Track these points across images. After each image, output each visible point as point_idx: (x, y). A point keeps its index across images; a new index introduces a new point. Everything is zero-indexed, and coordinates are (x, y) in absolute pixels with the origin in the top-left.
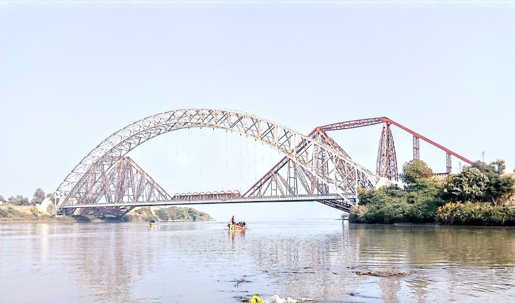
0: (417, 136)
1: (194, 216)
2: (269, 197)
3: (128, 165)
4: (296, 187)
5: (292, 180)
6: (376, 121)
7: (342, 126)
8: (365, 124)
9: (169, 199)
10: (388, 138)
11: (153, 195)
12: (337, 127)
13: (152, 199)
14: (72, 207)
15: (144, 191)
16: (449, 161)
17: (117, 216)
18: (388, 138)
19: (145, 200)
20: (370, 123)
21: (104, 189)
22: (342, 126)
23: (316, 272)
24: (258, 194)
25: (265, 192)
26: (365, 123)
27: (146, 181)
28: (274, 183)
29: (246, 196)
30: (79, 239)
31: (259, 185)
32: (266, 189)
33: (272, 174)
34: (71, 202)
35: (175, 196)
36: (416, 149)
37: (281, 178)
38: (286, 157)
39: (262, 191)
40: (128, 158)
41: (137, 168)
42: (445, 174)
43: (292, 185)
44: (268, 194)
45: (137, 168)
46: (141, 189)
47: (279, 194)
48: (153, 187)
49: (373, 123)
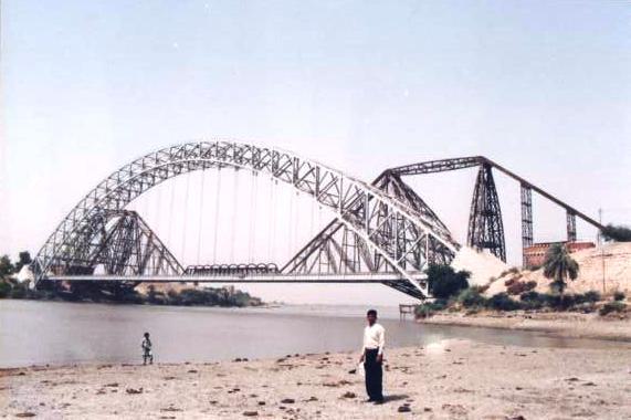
0: (526, 185)
3: (130, 222)
7: (423, 168)
10: (486, 185)
15: (151, 259)
17: (121, 295)
18: (486, 185)
19: (151, 273)
22: (423, 168)
23: (565, 384)
29: (287, 271)
31: (304, 255)
33: (322, 240)
36: (527, 205)
38: (336, 220)
43: (350, 257)
48: (162, 257)
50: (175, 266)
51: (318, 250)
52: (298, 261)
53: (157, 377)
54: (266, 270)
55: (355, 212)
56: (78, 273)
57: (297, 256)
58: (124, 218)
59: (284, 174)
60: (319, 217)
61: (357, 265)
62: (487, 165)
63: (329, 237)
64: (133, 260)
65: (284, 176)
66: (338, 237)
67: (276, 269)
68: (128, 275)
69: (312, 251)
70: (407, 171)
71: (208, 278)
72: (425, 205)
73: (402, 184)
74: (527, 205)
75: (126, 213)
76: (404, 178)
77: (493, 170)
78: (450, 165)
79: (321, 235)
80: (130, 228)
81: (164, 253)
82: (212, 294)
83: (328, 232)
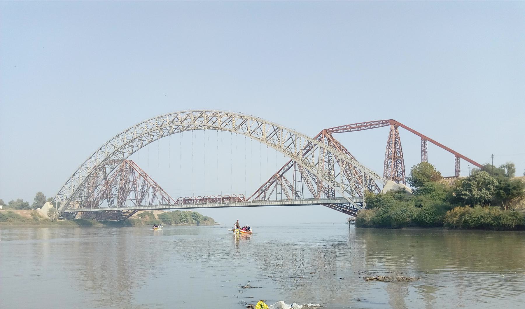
0: (425, 139)
1: (197, 220)
3: (128, 169)
4: (301, 191)
5: (298, 183)
6: (384, 123)
7: (348, 129)
8: (372, 127)
10: (395, 141)
12: (343, 129)
13: (155, 203)
14: (73, 211)
15: (147, 195)
16: (457, 164)
18: (395, 141)
19: (148, 204)
20: (378, 126)
21: (106, 194)
22: (348, 129)
24: (263, 198)
25: (270, 196)
27: (149, 185)
28: (279, 186)
29: (251, 200)
31: (264, 188)
32: (271, 193)
33: (277, 178)
35: (178, 200)
37: (286, 181)
39: (267, 195)
40: (131, 161)
44: (273, 197)
46: (143, 193)
47: (285, 198)
51: (276, 182)
52: (261, 192)
54: (236, 199)
56: (88, 207)
57: (260, 189)
62: (396, 124)
63: (281, 176)
64: (132, 195)
68: (129, 204)
76: (333, 135)
81: (156, 189)
82: (185, 216)
83: (281, 173)
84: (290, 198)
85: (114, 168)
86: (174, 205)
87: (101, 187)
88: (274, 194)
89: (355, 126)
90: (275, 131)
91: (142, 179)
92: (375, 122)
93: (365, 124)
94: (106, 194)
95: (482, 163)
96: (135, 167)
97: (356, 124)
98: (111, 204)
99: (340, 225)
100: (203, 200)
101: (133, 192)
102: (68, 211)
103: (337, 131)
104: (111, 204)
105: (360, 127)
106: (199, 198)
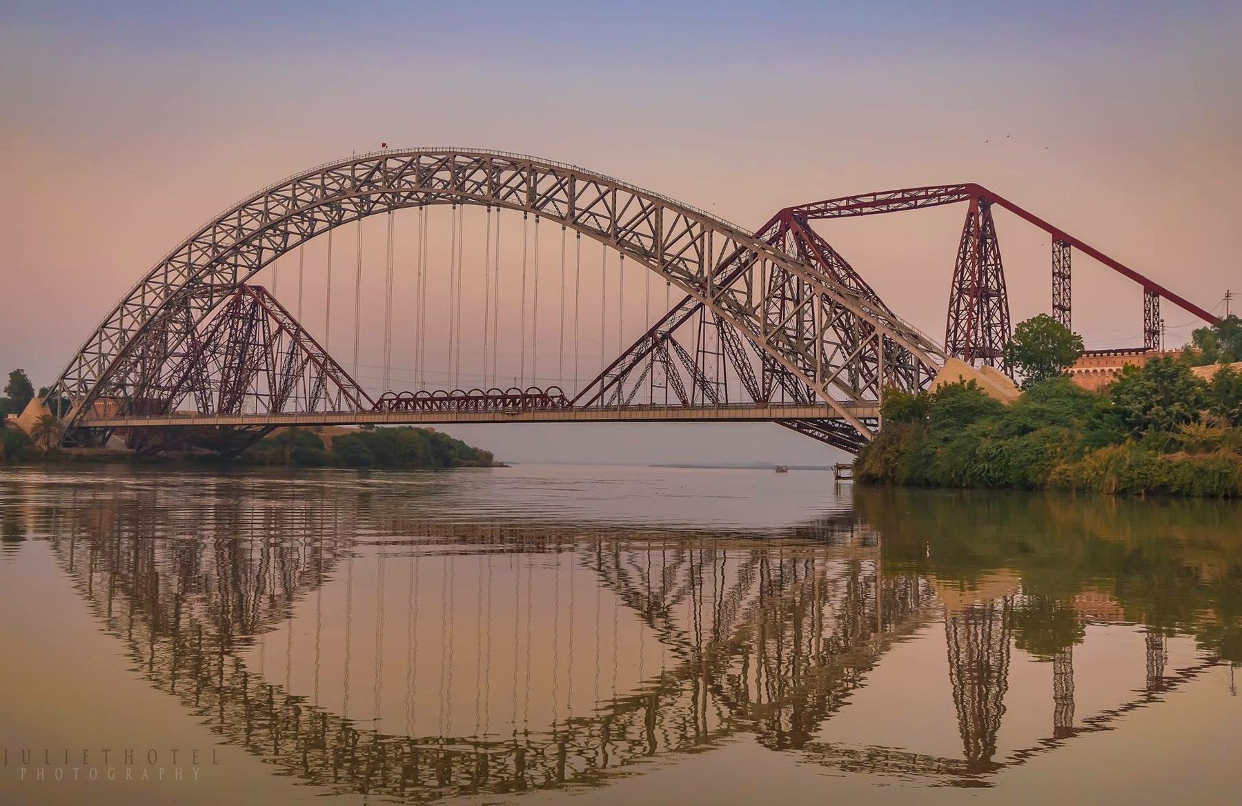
0: (1062, 240)
1: (449, 456)
2: (640, 407)
3: (250, 305)
4: (721, 380)
5: (711, 359)
6: (952, 194)
7: (855, 206)
8: (920, 202)
9: (368, 406)
10: (980, 240)
11: (323, 395)
12: (839, 208)
13: (320, 407)
14: (102, 424)
15: (301, 382)
16: (1151, 314)
18: (980, 240)
20: (935, 201)
21: (192, 380)
22: (855, 206)
24: (613, 398)
25: (634, 393)
26: (922, 197)
27: (305, 355)
28: (658, 366)
30: (216, 506)
31: (616, 371)
32: (638, 385)
33: (656, 340)
34: (101, 411)
35: (381, 401)
36: (1062, 276)
37: (680, 351)
39: (627, 388)
40: (259, 289)
41: (281, 317)
42: (1137, 351)
43: (710, 375)
44: (641, 398)
45: (281, 317)
46: (291, 378)
47: (674, 400)
49: (943, 198)
50: (353, 392)
52: (607, 380)
53: (743, 368)
55: (710, 289)
56: (141, 414)
58: (238, 301)
59: (550, 205)
60: (648, 295)
61: (722, 387)
62: (981, 198)
63: (666, 336)
64: (260, 383)
65: (550, 207)
66: (686, 335)
67: (562, 398)
69: (640, 357)
70: (824, 210)
71: (89, 480)
72: (853, 275)
73: (812, 236)
74: (1062, 276)
75: (243, 289)
77: (996, 209)
78: (909, 199)
79: (651, 333)
80: (251, 321)
81: (327, 367)
83: (664, 328)
84: (722, 401)
85: (211, 309)
86: (372, 412)
87: (177, 360)
88: (648, 385)
89: (871, 199)
90: (644, 210)
91: (286, 339)
92: (927, 189)
93: (899, 196)
94: (192, 380)
95: (1220, 313)
96: (269, 305)
97: (874, 194)
98: (205, 406)
99: (814, 481)
100: (467, 401)
101: (262, 376)
102: (91, 424)
103: (819, 211)
104: (205, 406)
105: (887, 202)
106: (454, 394)
